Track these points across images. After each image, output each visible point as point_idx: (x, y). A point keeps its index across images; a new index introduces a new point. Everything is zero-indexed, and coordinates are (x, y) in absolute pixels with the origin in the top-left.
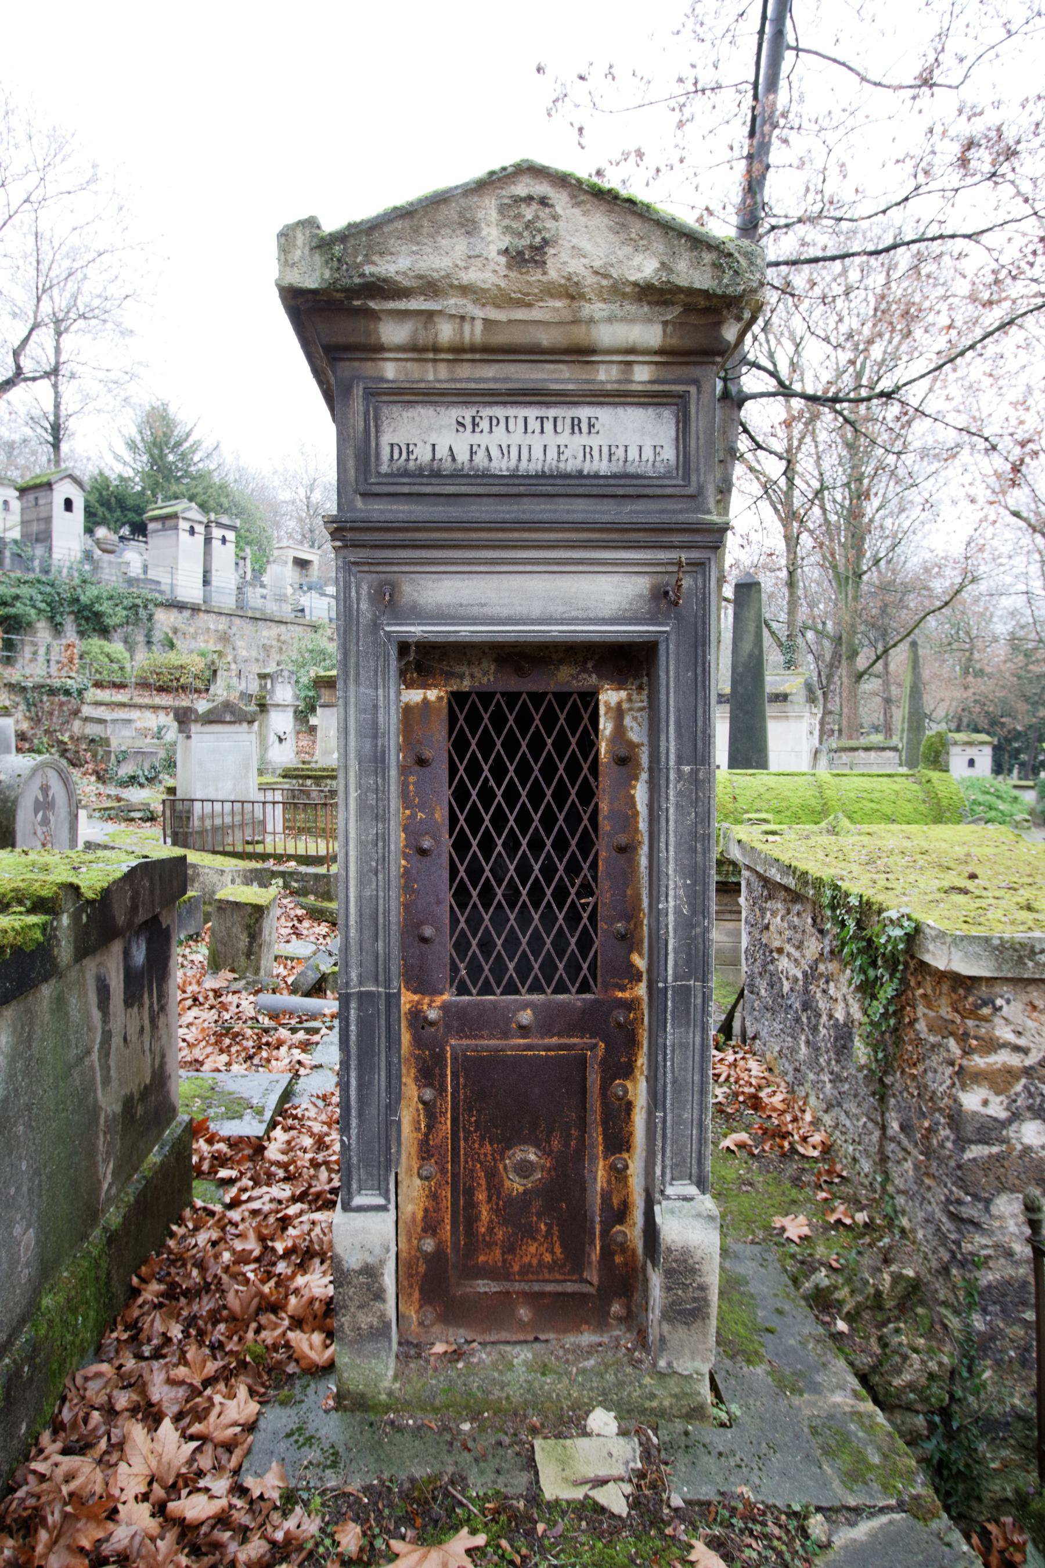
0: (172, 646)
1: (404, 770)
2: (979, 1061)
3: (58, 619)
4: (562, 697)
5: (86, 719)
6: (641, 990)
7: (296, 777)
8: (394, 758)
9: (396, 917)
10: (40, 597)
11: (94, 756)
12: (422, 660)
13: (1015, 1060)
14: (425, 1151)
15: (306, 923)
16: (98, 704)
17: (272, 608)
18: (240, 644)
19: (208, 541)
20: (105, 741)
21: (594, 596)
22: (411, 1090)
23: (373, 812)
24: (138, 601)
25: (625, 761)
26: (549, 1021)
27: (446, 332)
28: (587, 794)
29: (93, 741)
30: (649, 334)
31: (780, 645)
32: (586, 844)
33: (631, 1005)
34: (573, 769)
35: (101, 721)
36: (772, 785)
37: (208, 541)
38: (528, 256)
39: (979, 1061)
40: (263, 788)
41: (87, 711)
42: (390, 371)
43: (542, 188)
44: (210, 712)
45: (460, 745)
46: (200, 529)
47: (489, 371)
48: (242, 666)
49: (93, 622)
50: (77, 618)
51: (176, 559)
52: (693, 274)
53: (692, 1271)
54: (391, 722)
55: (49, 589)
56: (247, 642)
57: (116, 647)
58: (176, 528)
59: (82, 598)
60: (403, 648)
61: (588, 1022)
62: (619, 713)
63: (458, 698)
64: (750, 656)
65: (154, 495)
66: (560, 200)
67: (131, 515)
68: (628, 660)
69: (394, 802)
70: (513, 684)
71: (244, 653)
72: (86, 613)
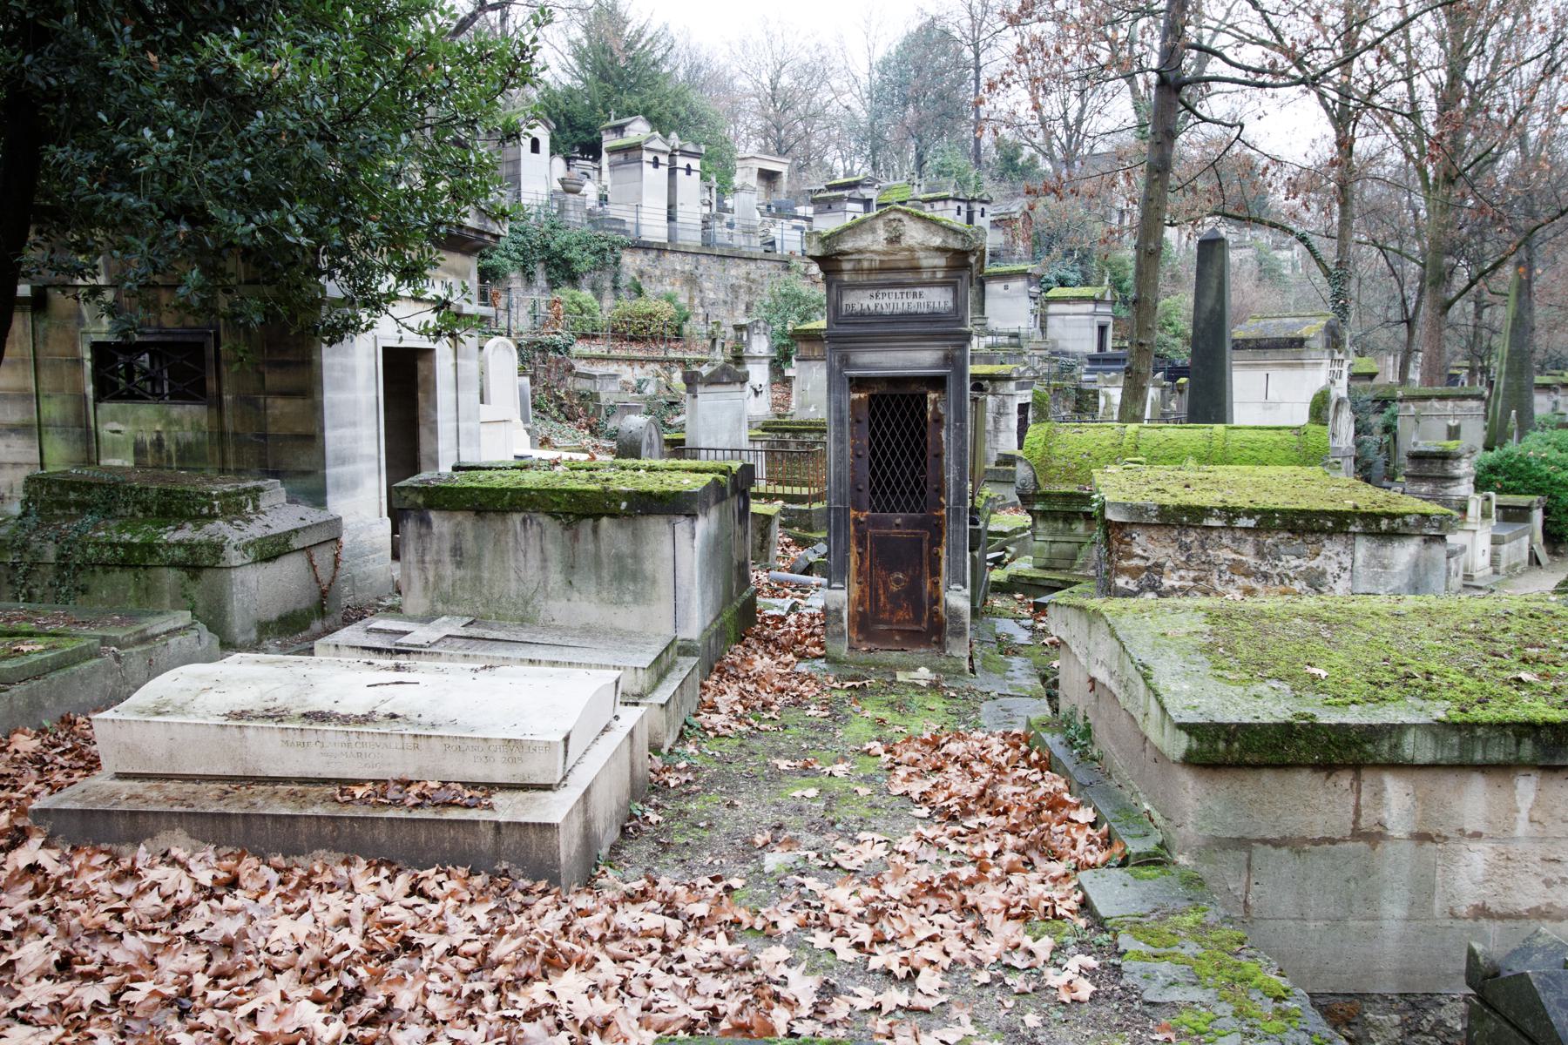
0: (640, 292)
1: (851, 425)
2: (1124, 563)
3: (530, 268)
4: (913, 396)
5: (579, 375)
6: (944, 512)
7: (775, 430)
8: (848, 420)
9: (848, 480)
10: (513, 247)
11: (586, 410)
12: (858, 383)
13: (1142, 563)
14: (859, 572)
15: (793, 548)
16: (591, 359)
17: (739, 241)
18: (707, 285)
19: (672, 171)
20: (595, 396)
21: (922, 359)
22: (854, 549)
23: (840, 440)
24: (605, 245)
25: (938, 420)
26: (908, 523)
27: (866, 265)
28: (923, 434)
29: (584, 396)
30: (941, 261)
31: (1327, 273)
32: (923, 454)
33: (941, 518)
34: (917, 425)
35: (590, 377)
36: (1172, 436)
37: (672, 171)
38: (894, 240)
39: (1124, 563)
40: (752, 440)
41: (581, 367)
42: (846, 278)
43: (899, 216)
44: (712, 375)
45: (873, 415)
46: (664, 159)
47: (882, 276)
48: (709, 309)
49: (562, 270)
50: (547, 266)
51: (640, 194)
52: (954, 243)
53: (959, 617)
54: (846, 406)
55: (521, 238)
56: (715, 280)
57: (585, 295)
58: (640, 160)
59: (553, 245)
60: (851, 379)
61: (920, 524)
62: (935, 402)
63: (872, 397)
64: (1212, 311)
65: (607, 111)
66: (906, 219)
67: (581, 135)
68: (937, 383)
69: (848, 436)
70: (894, 391)
71: (712, 295)
72: (556, 261)
